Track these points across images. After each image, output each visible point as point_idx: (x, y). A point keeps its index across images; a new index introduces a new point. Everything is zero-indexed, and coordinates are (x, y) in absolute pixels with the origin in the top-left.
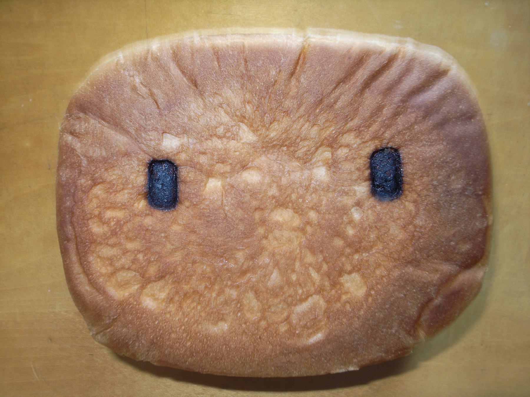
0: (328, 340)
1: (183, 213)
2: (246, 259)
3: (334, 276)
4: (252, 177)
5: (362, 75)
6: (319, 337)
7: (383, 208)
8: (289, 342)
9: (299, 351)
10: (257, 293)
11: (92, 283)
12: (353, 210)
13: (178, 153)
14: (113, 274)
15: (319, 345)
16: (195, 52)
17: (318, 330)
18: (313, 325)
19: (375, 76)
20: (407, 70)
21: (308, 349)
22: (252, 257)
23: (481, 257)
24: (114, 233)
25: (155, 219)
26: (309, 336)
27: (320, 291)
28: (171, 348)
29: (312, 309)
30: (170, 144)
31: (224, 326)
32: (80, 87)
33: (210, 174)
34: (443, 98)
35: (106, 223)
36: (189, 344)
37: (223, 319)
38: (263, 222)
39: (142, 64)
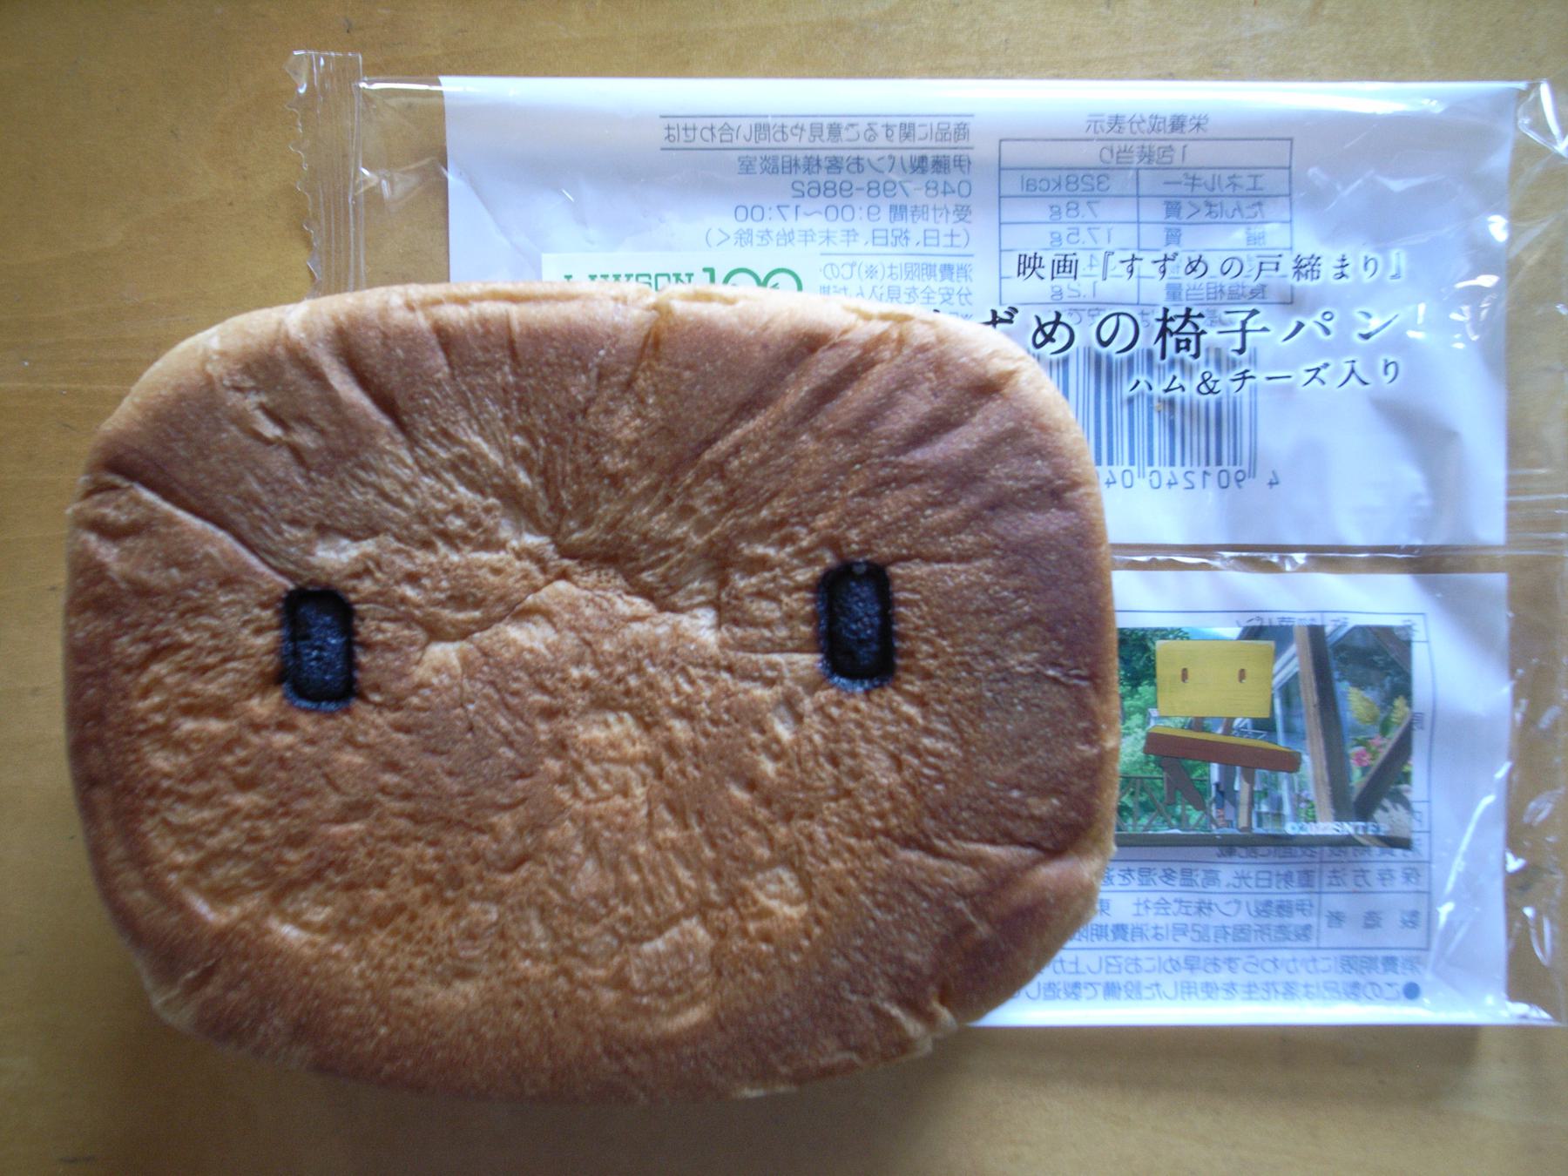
0: (718, 1022)
1: (370, 721)
2: (520, 830)
3: (731, 874)
4: (529, 637)
5: (795, 394)
6: (694, 1016)
7: (857, 703)
8: (622, 1027)
9: (647, 1048)
10: (544, 912)
11: (155, 886)
12: (273, 922)
13: (357, 576)
14: (201, 867)
15: (698, 1033)
16: (397, 338)
17: (694, 1001)
18: (676, 992)
19: (827, 393)
20: (906, 383)
21: (669, 1043)
22: (535, 826)
23: (1090, 825)
24: (202, 774)
25: (302, 735)
26: (675, 1011)
27: (703, 908)
28: (345, 1036)
29: (678, 951)
30: (335, 556)
31: (468, 991)
32: (123, 416)
33: (436, 633)
34: (993, 446)
35: (181, 745)
36: (383, 1031)
37: (464, 974)
38: (560, 746)
39: (272, 368)
